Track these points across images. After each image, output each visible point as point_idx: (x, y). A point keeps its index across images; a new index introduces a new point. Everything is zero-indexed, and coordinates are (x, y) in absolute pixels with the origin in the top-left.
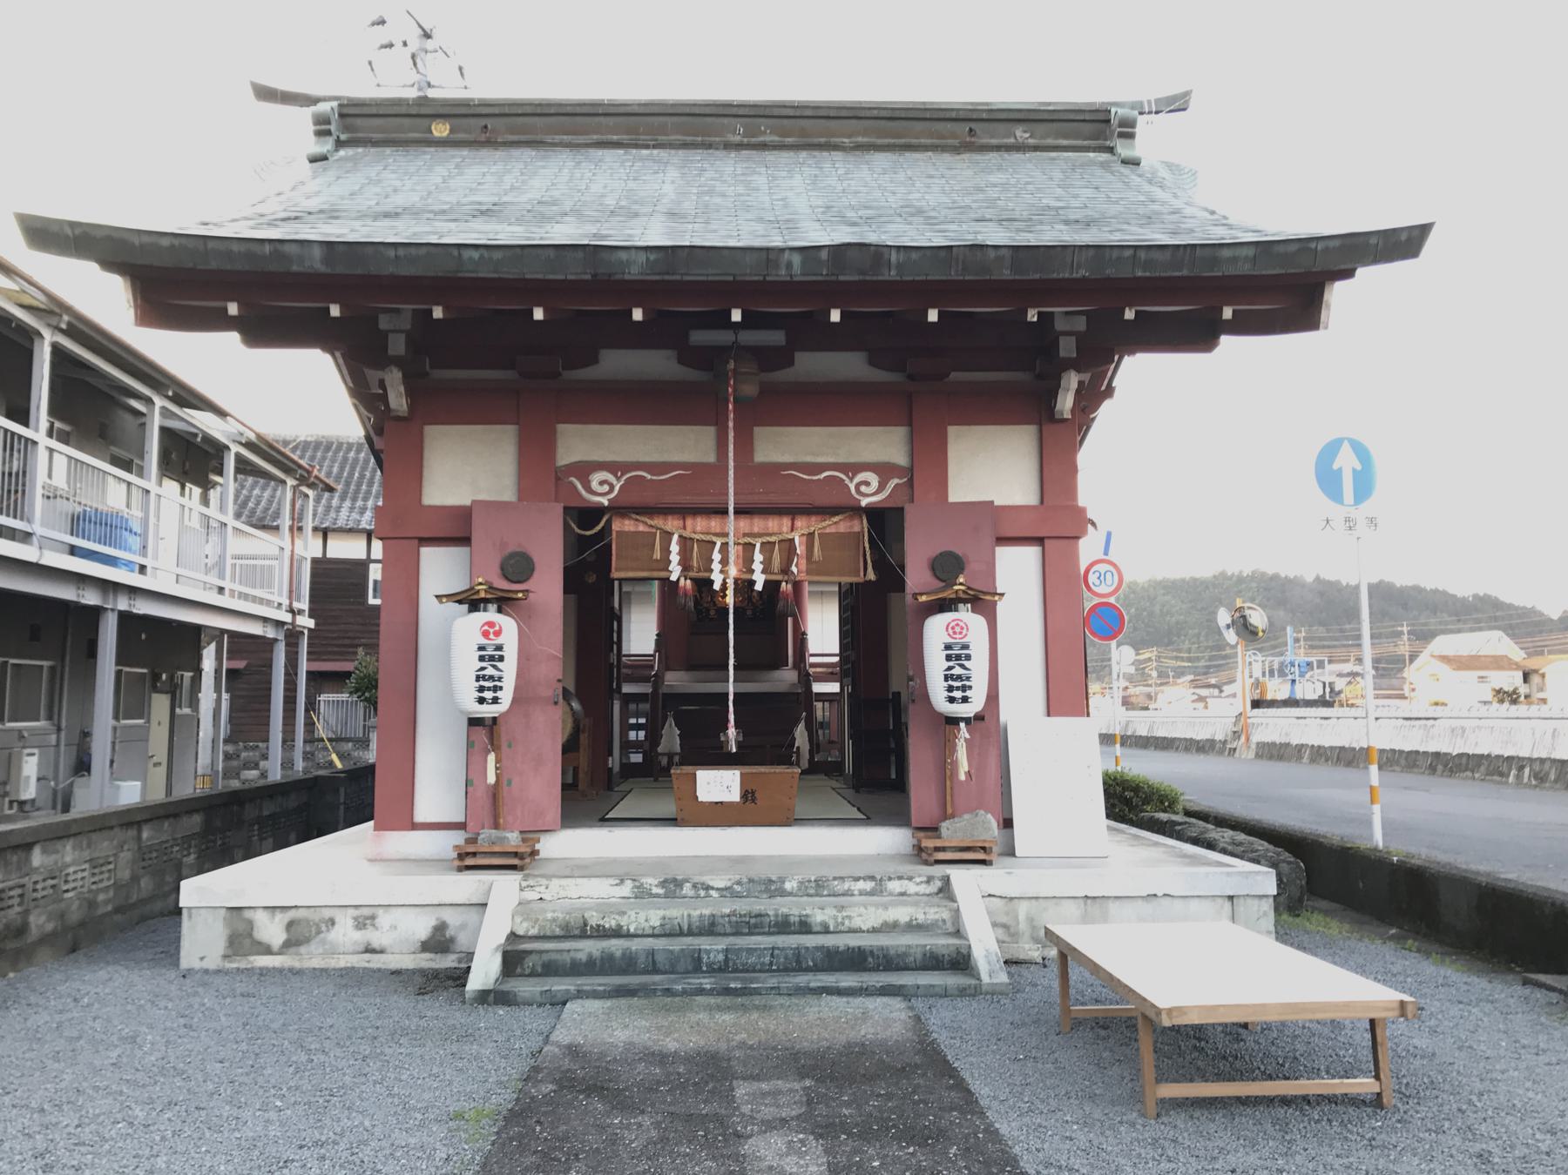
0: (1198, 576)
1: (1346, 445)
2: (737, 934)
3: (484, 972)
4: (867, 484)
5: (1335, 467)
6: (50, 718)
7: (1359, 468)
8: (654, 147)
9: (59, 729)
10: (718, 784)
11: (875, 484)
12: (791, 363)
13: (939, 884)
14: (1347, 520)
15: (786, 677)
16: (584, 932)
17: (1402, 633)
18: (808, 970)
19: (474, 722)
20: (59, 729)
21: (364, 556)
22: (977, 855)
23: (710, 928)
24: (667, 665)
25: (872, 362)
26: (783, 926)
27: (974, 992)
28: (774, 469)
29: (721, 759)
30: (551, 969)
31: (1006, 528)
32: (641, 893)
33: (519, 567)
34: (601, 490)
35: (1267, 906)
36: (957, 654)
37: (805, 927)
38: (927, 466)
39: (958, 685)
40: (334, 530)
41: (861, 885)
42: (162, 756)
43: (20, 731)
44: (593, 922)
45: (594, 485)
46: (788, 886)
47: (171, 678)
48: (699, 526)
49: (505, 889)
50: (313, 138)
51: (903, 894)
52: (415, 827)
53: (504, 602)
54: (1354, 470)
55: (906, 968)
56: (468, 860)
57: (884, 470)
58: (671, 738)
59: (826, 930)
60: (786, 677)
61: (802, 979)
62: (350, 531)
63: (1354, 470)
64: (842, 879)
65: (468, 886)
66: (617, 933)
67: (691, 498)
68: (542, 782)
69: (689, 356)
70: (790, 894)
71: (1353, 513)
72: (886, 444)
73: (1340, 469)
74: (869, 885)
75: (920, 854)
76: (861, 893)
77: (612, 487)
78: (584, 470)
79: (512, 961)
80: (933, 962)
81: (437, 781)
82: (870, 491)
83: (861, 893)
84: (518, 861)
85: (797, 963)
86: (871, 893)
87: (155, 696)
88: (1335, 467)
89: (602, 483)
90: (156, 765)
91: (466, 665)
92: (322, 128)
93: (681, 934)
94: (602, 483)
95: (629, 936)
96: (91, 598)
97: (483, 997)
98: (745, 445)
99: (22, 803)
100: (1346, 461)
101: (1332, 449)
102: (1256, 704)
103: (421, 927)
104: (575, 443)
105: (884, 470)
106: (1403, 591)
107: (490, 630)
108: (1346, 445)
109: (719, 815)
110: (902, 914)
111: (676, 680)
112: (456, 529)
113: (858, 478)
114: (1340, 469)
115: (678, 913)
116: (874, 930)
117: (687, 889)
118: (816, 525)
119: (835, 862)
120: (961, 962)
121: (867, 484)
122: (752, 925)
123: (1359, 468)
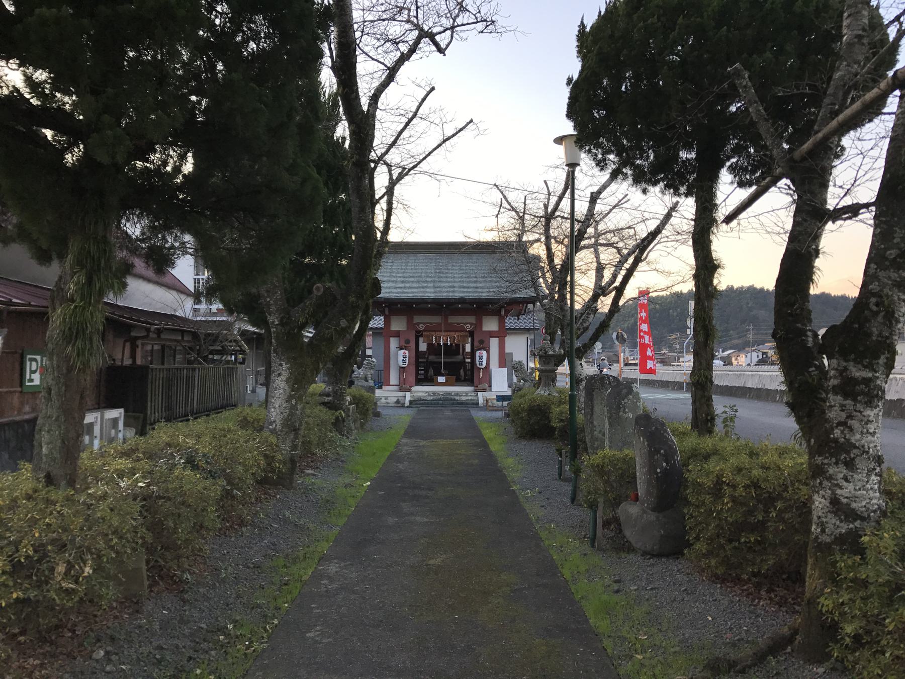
3: (407, 404)
10: (441, 379)
15: (460, 357)
17: (749, 330)
19: (401, 368)
22: (484, 390)
23: (440, 399)
24: (429, 354)
26: (451, 399)
28: (451, 324)
29: (442, 375)
31: (492, 334)
32: (429, 395)
33: (408, 342)
34: (421, 327)
36: (481, 357)
38: (479, 323)
39: (481, 362)
48: (438, 333)
49: (408, 394)
53: (406, 348)
56: (400, 390)
57: (471, 324)
58: (431, 372)
60: (460, 357)
65: (402, 394)
67: (436, 329)
68: (412, 379)
72: (472, 319)
75: (475, 391)
78: (418, 324)
79: (411, 402)
80: (473, 404)
81: (394, 378)
82: (468, 328)
84: (409, 390)
91: (401, 358)
98: (446, 319)
102: (626, 365)
103: (395, 399)
104: (417, 319)
105: (471, 324)
106: (836, 298)
107: (405, 353)
109: (442, 384)
111: (432, 358)
112: (397, 334)
118: (459, 334)
119: (462, 391)
120: (478, 404)
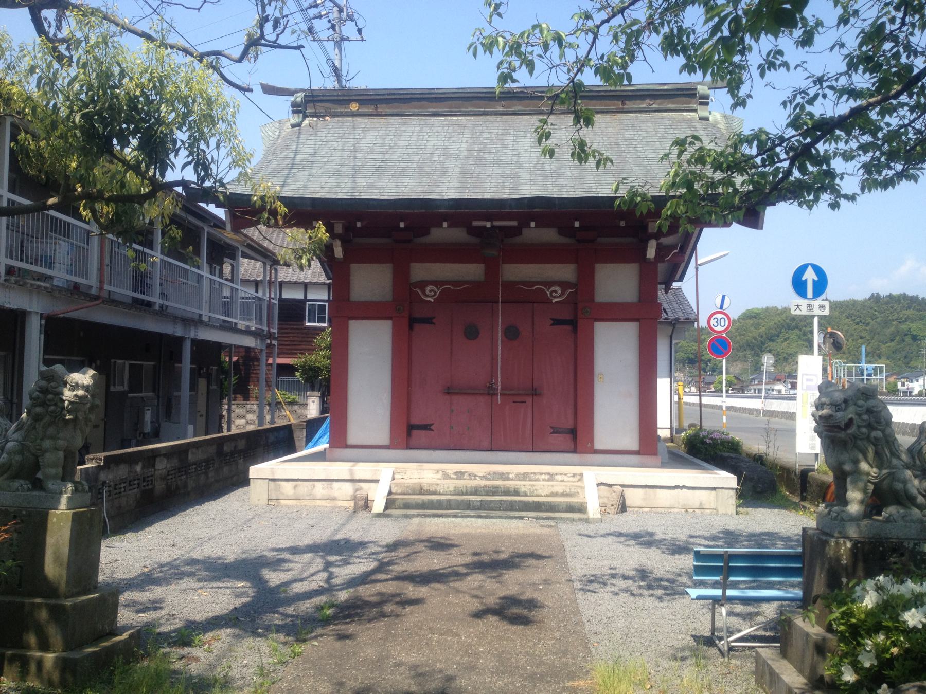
0: (856, 298)
1: (810, 267)
2: (487, 495)
3: (378, 506)
4: (556, 292)
5: (803, 278)
6: (154, 391)
7: (816, 279)
8: (460, 115)
9: (158, 397)
11: (559, 292)
12: (521, 234)
13: (578, 477)
14: (809, 306)
16: (421, 491)
18: (516, 510)
20: (158, 397)
21: (303, 297)
23: (475, 491)
25: (560, 233)
26: (507, 492)
27: (587, 521)
30: (407, 506)
35: (733, 493)
37: (516, 493)
40: (286, 283)
41: (543, 476)
42: (204, 413)
43: (142, 398)
44: (425, 488)
45: (427, 292)
46: (511, 476)
47: (207, 370)
50: (290, 113)
51: (562, 481)
52: (347, 446)
54: (814, 280)
55: (559, 511)
59: (526, 495)
61: (512, 513)
62: (295, 283)
63: (814, 280)
64: (535, 474)
66: (435, 493)
69: (472, 231)
70: (512, 480)
71: (812, 302)
72: (566, 272)
73: (806, 280)
74: (547, 477)
76: (544, 480)
77: (435, 293)
78: (423, 284)
79: (390, 504)
83: (544, 480)
85: (512, 507)
86: (548, 480)
87: (200, 380)
88: (803, 278)
89: (431, 291)
90: (201, 416)
92: (297, 108)
93: (463, 494)
94: (431, 291)
95: (440, 494)
96: (179, 331)
97: (379, 515)
99: (144, 434)
100: (810, 276)
101: (802, 270)
104: (420, 271)
105: (564, 285)
108: (810, 267)
110: (559, 489)
113: (553, 289)
114: (806, 280)
115: (461, 483)
116: (547, 496)
117: (466, 476)
120: (581, 509)
121: (556, 292)
122: (494, 491)
123: (816, 279)
